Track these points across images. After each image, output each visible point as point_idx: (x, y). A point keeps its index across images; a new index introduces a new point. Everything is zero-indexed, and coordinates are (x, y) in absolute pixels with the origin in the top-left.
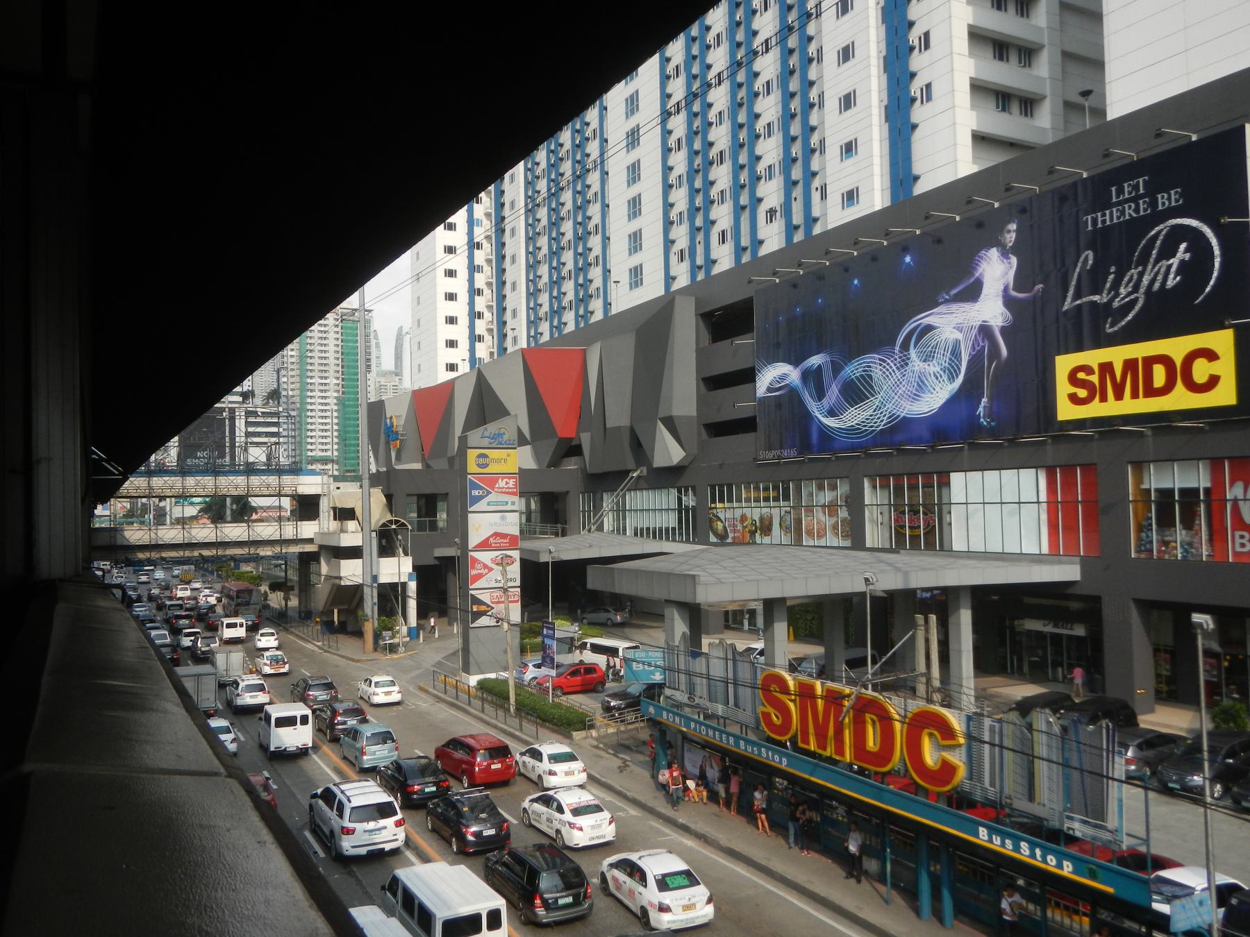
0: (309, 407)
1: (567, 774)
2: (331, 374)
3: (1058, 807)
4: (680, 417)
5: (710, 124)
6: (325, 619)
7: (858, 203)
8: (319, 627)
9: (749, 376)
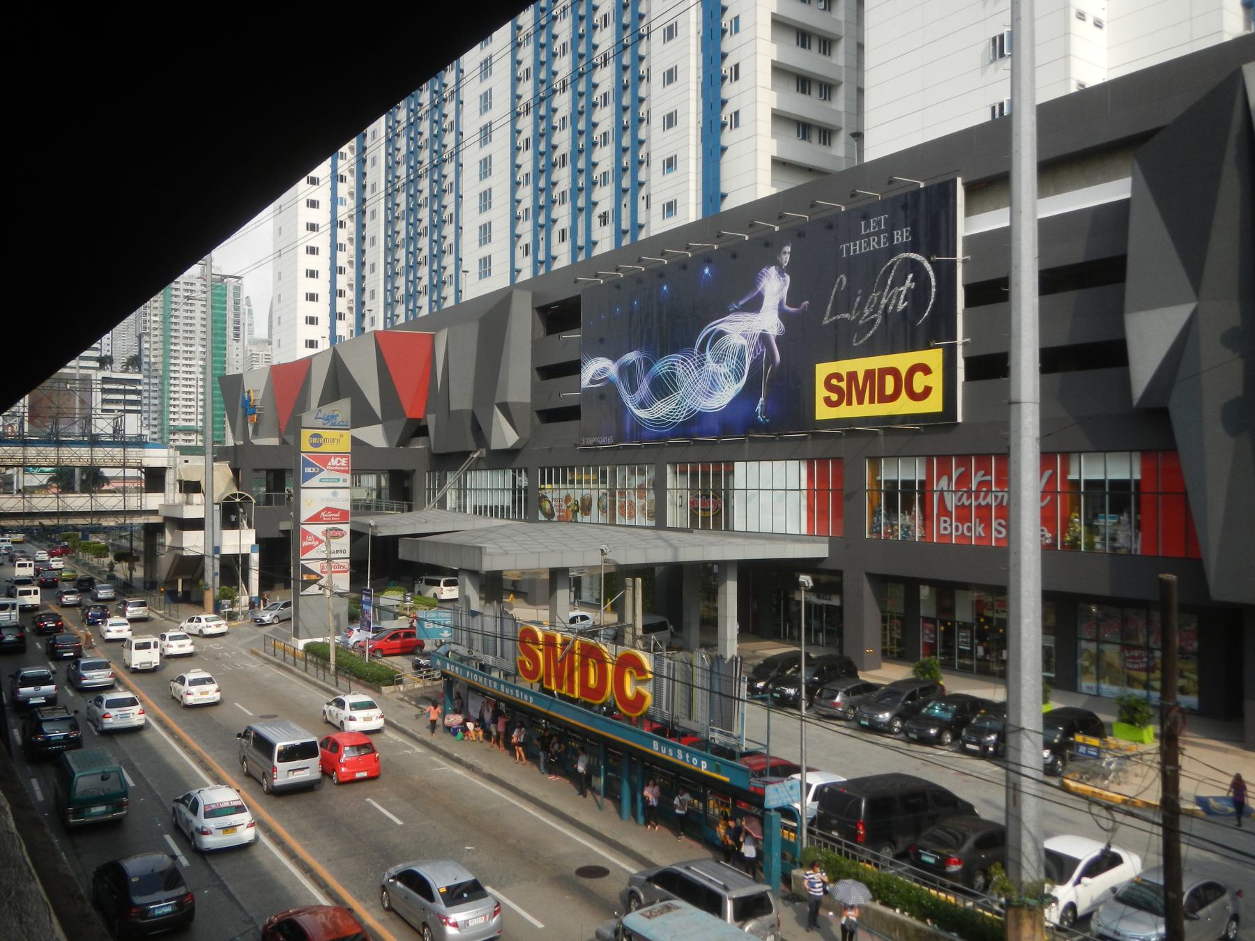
0: (173, 375)
1: (366, 719)
2: (197, 341)
3: (706, 722)
5: (555, 128)
6: (169, 589)
8: (162, 597)
9: (574, 368)
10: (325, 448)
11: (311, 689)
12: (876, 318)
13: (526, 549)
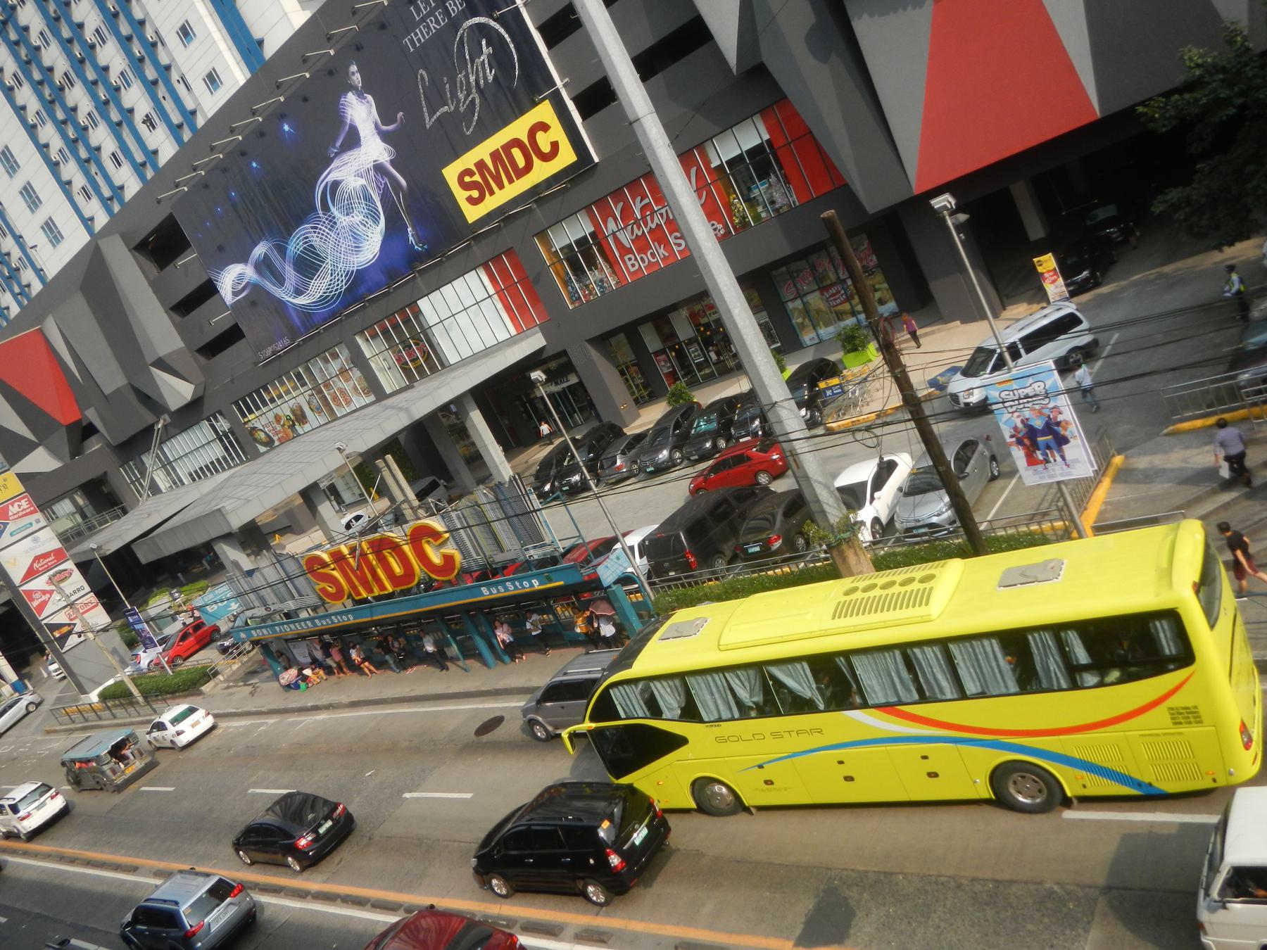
1: (193, 726)
3: (518, 546)
4: (169, 355)
7: (222, 83)
9: (208, 290)
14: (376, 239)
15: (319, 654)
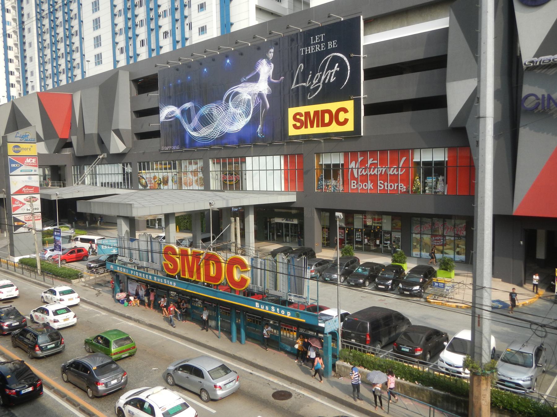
1: (69, 300)
3: (286, 291)
9: (156, 111)
10: (22, 153)
11: (29, 284)
12: (319, 86)
13: (153, 204)
14: (242, 123)
15: (142, 292)
